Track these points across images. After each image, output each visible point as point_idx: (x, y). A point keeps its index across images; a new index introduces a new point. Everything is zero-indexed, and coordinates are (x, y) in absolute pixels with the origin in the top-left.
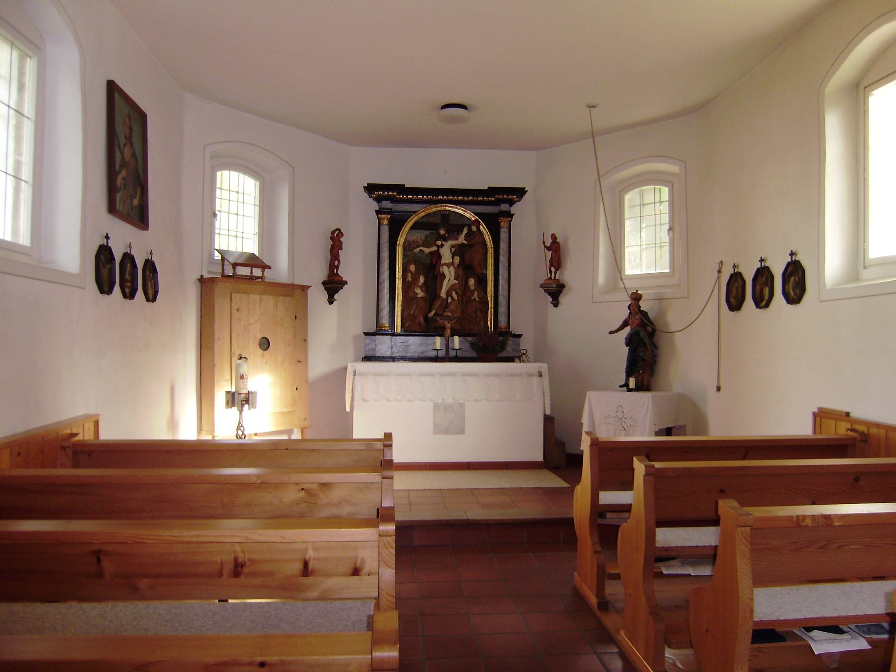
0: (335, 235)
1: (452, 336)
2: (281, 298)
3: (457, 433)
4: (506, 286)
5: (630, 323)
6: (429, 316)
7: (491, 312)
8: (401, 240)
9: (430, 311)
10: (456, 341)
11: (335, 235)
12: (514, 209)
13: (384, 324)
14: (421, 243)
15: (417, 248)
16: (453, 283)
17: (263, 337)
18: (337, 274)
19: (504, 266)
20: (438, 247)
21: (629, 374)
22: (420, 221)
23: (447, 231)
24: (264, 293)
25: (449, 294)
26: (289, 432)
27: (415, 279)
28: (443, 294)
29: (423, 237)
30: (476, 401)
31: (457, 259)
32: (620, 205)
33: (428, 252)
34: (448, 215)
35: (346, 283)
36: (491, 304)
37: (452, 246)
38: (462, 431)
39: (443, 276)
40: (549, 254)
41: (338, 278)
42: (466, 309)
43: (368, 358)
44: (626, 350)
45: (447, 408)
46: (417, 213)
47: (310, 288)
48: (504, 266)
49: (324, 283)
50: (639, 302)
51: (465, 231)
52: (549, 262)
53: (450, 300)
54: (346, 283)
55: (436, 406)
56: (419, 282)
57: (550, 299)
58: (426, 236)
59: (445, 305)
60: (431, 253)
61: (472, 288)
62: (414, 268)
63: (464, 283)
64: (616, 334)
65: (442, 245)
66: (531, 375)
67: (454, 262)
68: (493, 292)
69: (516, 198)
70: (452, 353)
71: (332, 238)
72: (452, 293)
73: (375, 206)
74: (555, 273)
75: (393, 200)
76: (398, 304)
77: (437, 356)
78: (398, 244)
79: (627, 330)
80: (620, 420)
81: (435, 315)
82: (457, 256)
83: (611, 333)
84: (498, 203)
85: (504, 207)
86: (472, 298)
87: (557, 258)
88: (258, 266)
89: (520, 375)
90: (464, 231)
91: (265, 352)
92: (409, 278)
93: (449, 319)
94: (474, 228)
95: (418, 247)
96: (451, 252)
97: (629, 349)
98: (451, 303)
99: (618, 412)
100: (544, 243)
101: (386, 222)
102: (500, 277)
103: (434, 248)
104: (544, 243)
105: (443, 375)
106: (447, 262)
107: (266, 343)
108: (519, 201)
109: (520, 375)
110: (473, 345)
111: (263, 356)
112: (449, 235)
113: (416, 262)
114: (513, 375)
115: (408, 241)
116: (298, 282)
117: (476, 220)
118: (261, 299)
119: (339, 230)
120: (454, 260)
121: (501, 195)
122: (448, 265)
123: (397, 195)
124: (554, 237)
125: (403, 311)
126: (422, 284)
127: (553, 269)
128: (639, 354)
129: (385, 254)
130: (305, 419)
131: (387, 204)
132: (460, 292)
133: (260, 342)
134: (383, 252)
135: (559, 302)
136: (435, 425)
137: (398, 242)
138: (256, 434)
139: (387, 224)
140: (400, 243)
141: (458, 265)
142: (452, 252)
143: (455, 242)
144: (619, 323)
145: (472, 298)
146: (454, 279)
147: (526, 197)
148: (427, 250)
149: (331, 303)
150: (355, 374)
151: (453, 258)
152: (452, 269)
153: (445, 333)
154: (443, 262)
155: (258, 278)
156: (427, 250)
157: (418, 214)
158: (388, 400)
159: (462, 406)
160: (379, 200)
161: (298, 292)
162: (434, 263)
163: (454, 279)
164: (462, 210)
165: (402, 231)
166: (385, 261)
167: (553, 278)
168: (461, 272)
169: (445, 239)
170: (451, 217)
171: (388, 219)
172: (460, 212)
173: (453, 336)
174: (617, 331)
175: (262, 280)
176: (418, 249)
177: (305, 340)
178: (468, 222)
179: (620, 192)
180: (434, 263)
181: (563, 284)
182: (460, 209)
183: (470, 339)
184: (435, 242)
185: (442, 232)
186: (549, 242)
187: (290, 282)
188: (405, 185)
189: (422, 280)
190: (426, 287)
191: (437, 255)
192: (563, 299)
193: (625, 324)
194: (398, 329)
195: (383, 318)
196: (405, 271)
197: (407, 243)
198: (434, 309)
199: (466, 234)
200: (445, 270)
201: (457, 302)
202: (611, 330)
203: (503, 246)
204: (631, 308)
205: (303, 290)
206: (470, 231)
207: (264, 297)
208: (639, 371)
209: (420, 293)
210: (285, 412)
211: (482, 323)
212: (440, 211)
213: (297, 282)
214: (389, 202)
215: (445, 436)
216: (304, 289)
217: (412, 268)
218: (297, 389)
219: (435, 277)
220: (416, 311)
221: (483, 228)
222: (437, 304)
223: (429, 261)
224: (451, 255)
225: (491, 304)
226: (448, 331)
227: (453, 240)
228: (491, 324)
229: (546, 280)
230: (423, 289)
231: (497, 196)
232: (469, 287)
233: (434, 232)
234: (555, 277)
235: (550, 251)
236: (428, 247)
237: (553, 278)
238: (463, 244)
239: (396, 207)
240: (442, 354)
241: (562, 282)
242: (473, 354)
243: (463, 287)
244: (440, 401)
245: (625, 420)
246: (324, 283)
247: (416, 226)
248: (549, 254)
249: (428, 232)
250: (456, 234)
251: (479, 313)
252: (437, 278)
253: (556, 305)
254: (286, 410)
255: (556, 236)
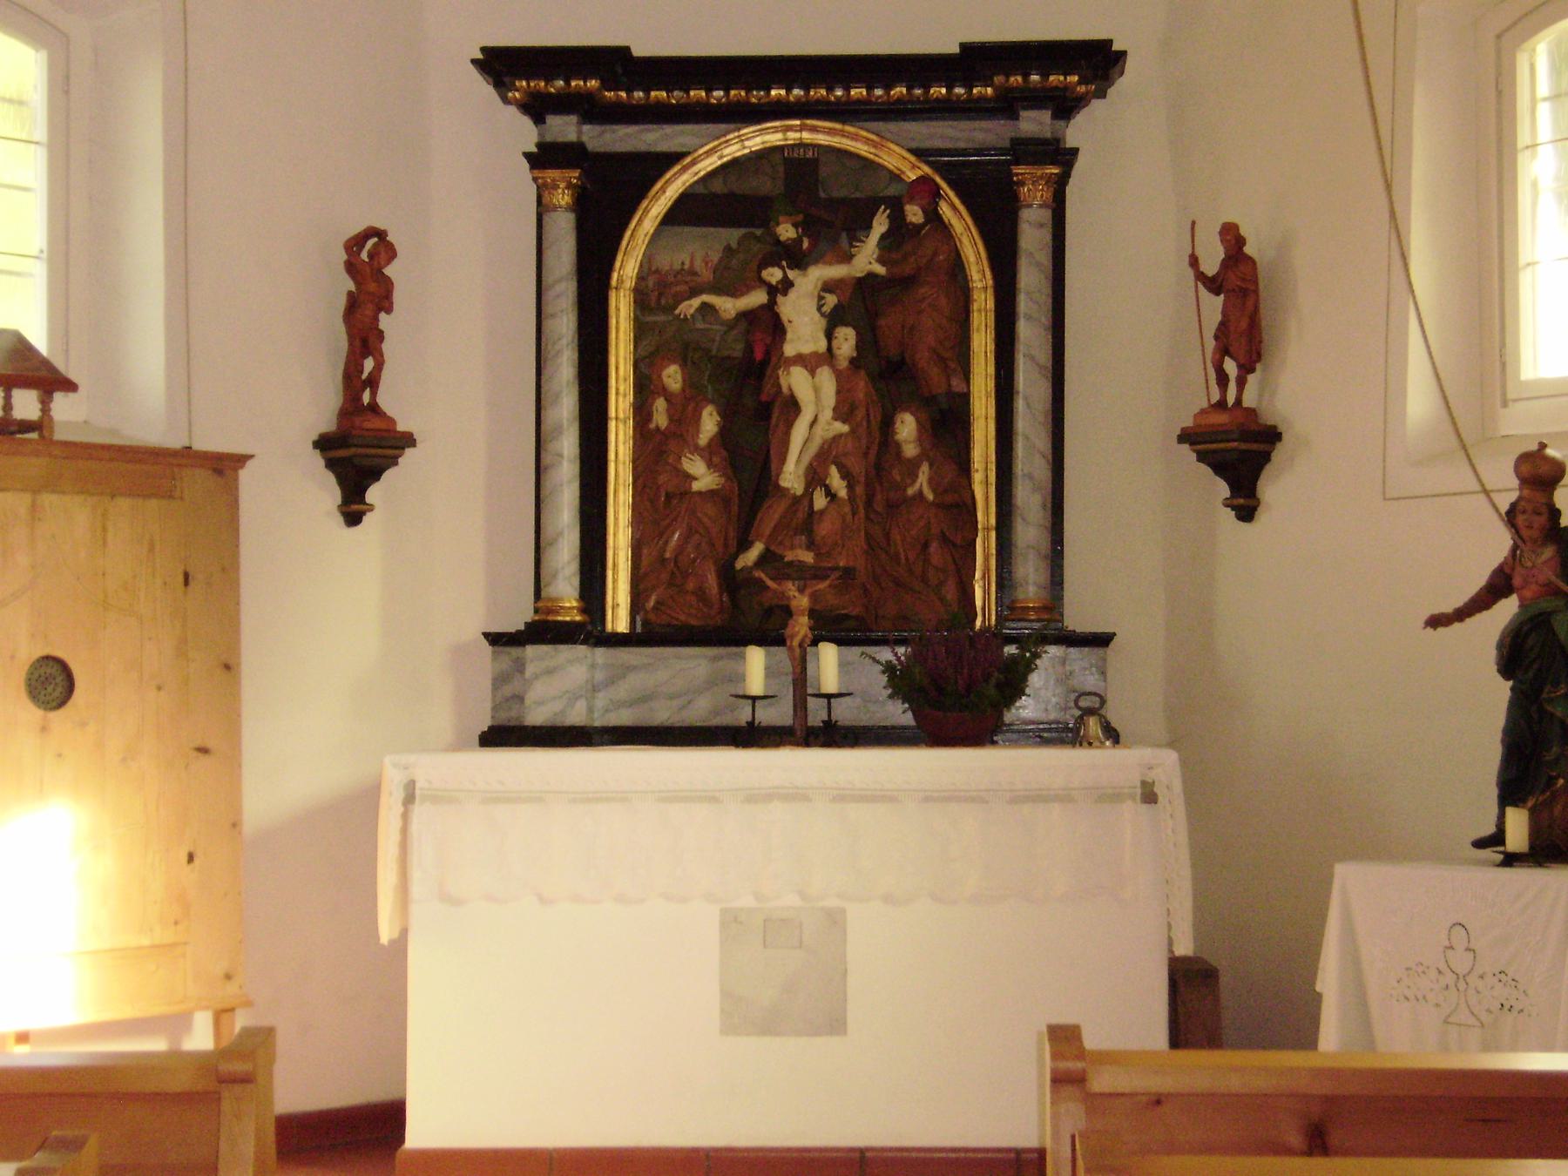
0: (364, 256)
1: (815, 643)
2: (124, 503)
3: (816, 1032)
4: (1043, 442)
5: (1517, 581)
6: (739, 564)
7: (985, 547)
8: (627, 268)
9: (744, 545)
10: (829, 664)
11: (364, 256)
12: (1077, 132)
13: (562, 599)
14: (706, 275)
15: (689, 298)
16: (830, 435)
17: (47, 658)
18: (374, 408)
19: (1032, 358)
20: (775, 291)
21: (1510, 793)
22: (701, 190)
23: (807, 225)
24: (50, 484)
25: (815, 477)
26: (179, 1022)
27: (684, 419)
28: (791, 477)
29: (715, 257)
30: (888, 899)
31: (846, 341)
32: (1499, 93)
33: (733, 314)
34: (814, 163)
35: (408, 440)
36: (986, 515)
37: (828, 287)
38: (836, 1024)
39: (792, 406)
40: (1214, 305)
41: (374, 423)
42: (887, 536)
43: (500, 736)
44: (1502, 690)
45: (775, 929)
46: (688, 160)
47: (250, 463)
48: (1032, 358)
49: (324, 444)
50: (1552, 494)
51: (880, 225)
52: (1216, 337)
53: (820, 501)
54: (408, 440)
55: (731, 922)
56: (698, 432)
57: (1223, 489)
58: (728, 250)
59: (803, 521)
60: (748, 316)
61: (910, 450)
62: (679, 377)
63: (877, 434)
64: (1457, 625)
65: (786, 285)
66: (1109, 797)
67: (837, 352)
68: (993, 467)
69: (1080, 83)
70: (817, 714)
71: (351, 268)
72: (827, 474)
73: (524, 134)
74: (1241, 383)
75: (593, 111)
76: (616, 519)
77: (751, 724)
78: (614, 282)
79: (1507, 610)
80: (1462, 985)
81: (762, 561)
82: (846, 325)
83: (1436, 622)
84: (1007, 106)
85: (1034, 123)
86: (910, 491)
87: (1244, 324)
88: (26, 383)
89: (1064, 797)
90: (875, 223)
91: (53, 715)
92: (660, 418)
93: (804, 575)
94: (914, 214)
95: (694, 292)
96: (819, 308)
97: (1512, 689)
98: (822, 512)
99: (1451, 948)
100: (1194, 261)
101: (563, 198)
102: (1020, 405)
103: (757, 298)
104: (1194, 261)
105: (796, 796)
106: (806, 349)
107: (60, 679)
108: (1101, 94)
109: (1064, 797)
110: (900, 682)
111: (44, 729)
112: (813, 245)
113: (687, 353)
114: (1039, 797)
115: (657, 271)
116: (207, 442)
117: (923, 180)
118: (34, 508)
119: (380, 234)
120: (835, 343)
121: (558, 77)
122: (810, 363)
123: (1080, 83)
124: (1232, 238)
125: (637, 548)
126: (712, 440)
127: (1230, 367)
128: (1549, 708)
129: (564, 325)
130: (228, 977)
131: (564, 128)
132: (858, 467)
133: (30, 673)
134: (553, 316)
135: (1258, 502)
136: (727, 994)
137: (615, 276)
138: (22, 1038)
139: (569, 208)
140: (621, 281)
141: (852, 361)
142: (827, 309)
143: (837, 271)
144: (1477, 580)
145: (910, 491)
146: (835, 418)
147: (1125, 84)
148: (729, 306)
149: (353, 516)
150: (409, 799)
151: (829, 335)
152: (827, 380)
153: (788, 632)
154: (789, 350)
155: (27, 426)
156: (729, 306)
157: (694, 163)
158: (543, 900)
159: (835, 920)
160: (536, 108)
161: (197, 481)
162: (759, 354)
163: (835, 418)
164: (867, 141)
165: (628, 233)
166: (559, 352)
167: (1231, 400)
168: (862, 387)
169: (796, 258)
170: (823, 172)
171: (569, 186)
172: (862, 149)
173: (817, 645)
174: (1462, 614)
175: (42, 436)
176: (696, 302)
177: (227, 667)
178: (893, 190)
179: (1499, 37)
180: (759, 354)
181: (1275, 427)
182: (855, 137)
183: (885, 654)
184: (759, 272)
185: (786, 231)
186: (1211, 263)
187: (175, 442)
188: (1111, 42)
189: (709, 424)
190: (727, 450)
191: (768, 323)
192: (1273, 489)
193: (1498, 587)
194: (619, 619)
195: (554, 576)
196: (645, 387)
197: (651, 282)
198: (759, 537)
199: (883, 237)
200: (797, 381)
201: (847, 509)
202: (1436, 611)
203: (1031, 279)
204: (1521, 520)
205: (219, 472)
206: (899, 232)
207: (48, 499)
208: (1551, 781)
209: (703, 476)
210: (140, 948)
211: (950, 592)
212: (780, 149)
213: (201, 444)
214: (573, 119)
215: (766, 1041)
216: (225, 466)
217: (673, 376)
218: (191, 858)
219: (763, 412)
220: (690, 548)
221: (955, 214)
222: (771, 515)
223: (737, 350)
224: (823, 323)
225: (986, 515)
226: (801, 626)
227: (830, 264)
228: (986, 592)
229: (1203, 412)
230: (716, 460)
231: (999, 79)
232: (898, 445)
233: (758, 232)
234: (1238, 401)
235: (1218, 294)
236: (734, 292)
237: (1231, 400)
238: (871, 275)
239: (608, 137)
240: (778, 714)
241: (1268, 418)
242: (899, 714)
243: (875, 447)
244: (747, 901)
245: (1480, 984)
246: (324, 444)
247: (685, 212)
248: (1214, 305)
249: (733, 235)
250: (844, 237)
251: (934, 547)
252: (769, 418)
253: (1246, 513)
254: (146, 941)
255: (1243, 232)
